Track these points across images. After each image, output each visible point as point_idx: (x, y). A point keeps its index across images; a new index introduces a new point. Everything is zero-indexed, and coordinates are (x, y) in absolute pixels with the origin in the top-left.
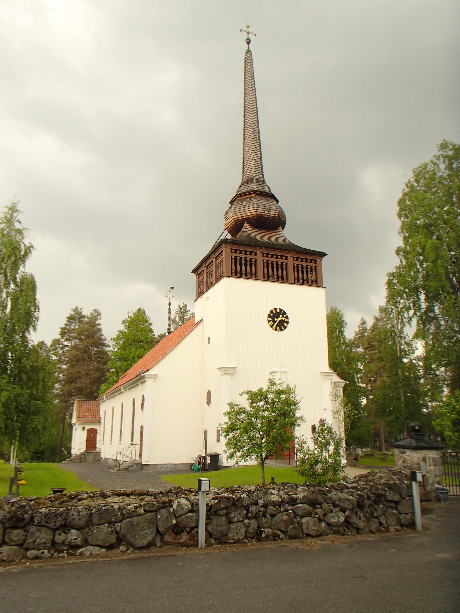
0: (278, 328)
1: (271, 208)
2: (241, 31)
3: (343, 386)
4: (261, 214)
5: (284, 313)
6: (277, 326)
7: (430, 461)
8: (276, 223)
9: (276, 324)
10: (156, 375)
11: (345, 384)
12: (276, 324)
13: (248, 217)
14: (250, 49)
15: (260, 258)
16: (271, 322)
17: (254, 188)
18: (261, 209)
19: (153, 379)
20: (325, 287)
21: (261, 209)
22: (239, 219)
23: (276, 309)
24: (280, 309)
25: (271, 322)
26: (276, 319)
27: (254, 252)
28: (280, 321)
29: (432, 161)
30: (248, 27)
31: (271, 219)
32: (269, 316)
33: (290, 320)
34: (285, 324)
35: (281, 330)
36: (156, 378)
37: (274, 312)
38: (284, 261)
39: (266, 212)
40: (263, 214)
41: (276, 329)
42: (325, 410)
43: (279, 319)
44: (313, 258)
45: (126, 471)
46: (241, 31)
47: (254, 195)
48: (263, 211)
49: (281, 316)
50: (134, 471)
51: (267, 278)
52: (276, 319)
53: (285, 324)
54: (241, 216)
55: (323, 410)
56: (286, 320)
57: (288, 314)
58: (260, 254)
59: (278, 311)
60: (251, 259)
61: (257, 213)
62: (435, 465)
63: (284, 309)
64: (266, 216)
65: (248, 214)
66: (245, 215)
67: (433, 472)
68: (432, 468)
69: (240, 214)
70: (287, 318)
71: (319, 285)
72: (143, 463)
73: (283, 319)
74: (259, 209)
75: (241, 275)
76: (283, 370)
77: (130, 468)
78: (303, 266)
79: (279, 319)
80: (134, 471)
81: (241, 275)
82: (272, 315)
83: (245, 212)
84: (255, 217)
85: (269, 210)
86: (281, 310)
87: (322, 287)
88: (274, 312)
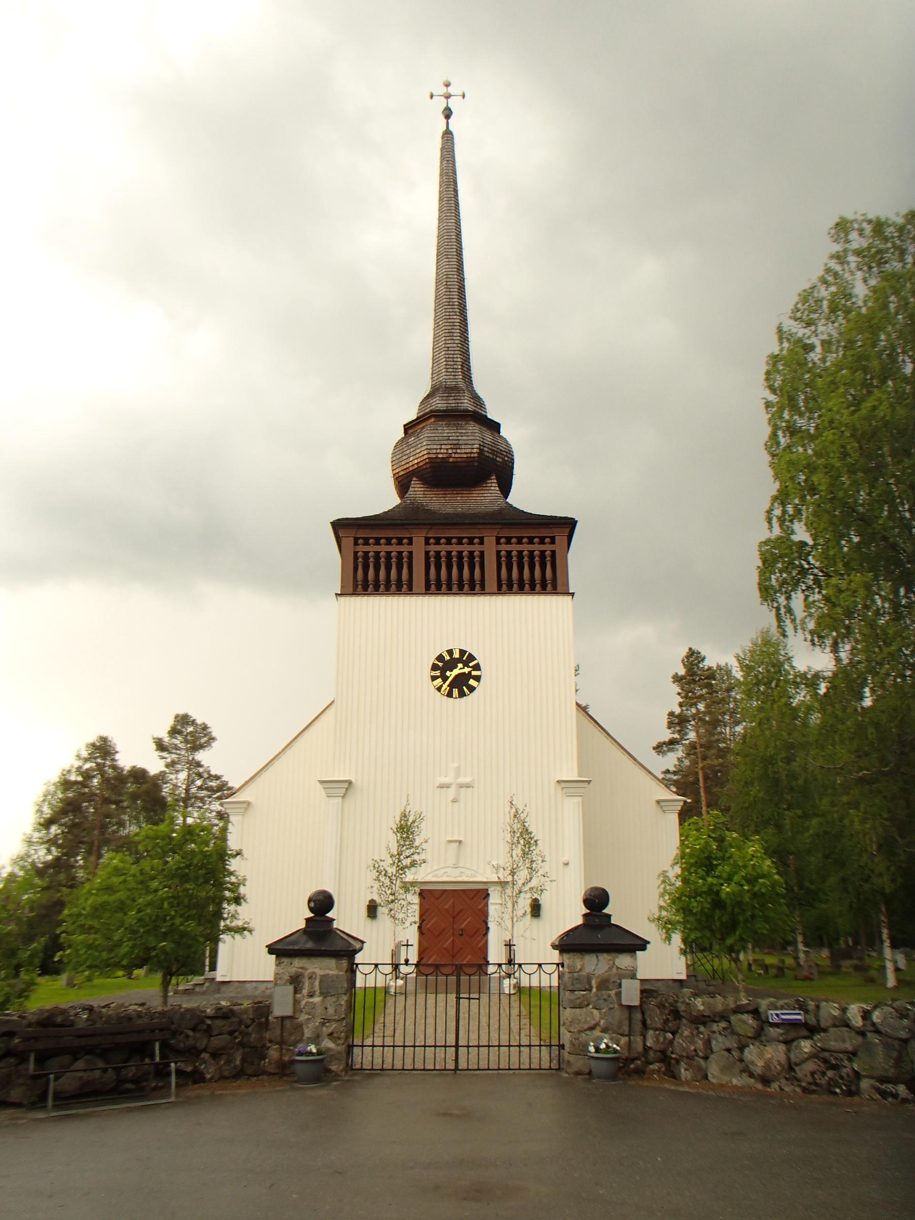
0: (455, 692)
1: (461, 442)
2: (432, 96)
3: (679, 808)
4: (440, 456)
5: (471, 658)
6: (451, 686)
7: (312, 984)
8: (497, 467)
9: (448, 683)
10: (248, 804)
11: (682, 804)
12: (448, 683)
13: (416, 466)
14: (450, 128)
15: (490, 548)
16: (440, 680)
17: (453, 405)
18: (439, 447)
19: (242, 810)
20: (573, 594)
21: (439, 447)
22: (402, 473)
23: (450, 652)
24: (460, 650)
25: (440, 680)
26: (448, 673)
27: (407, 538)
28: (456, 676)
29: (828, 270)
30: (447, 85)
31: (463, 464)
32: (434, 667)
33: (484, 673)
34: (472, 682)
35: (462, 694)
36: (246, 809)
37: (447, 658)
38: (477, 548)
39: (450, 451)
40: (445, 456)
41: (450, 695)
42: (567, 864)
43: (456, 672)
44: (544, 532)
45: (189, 994)
46: (432, 96)
47: (433, 420)
48: (442, 451)
49: (460, 665)
50: (204, 993)
51: (506, 587)
52: (448, 673)
53: (472, 682)
54: (405, 467)
55: (561, 865)
56: (474, 673)
57: (480, 659)
58: (490, 541)
59: (456, 655)
60: (400, 553)
61: (431, 456)
62: (324, 994)
63: (469, 650)
64: (451, 460)
65: (416, 461)
66: (411, 464)
67: (319, 1011)
68: (317, 999)
69: (403, 463)
70: (477, 667)
71: (559, 589)
72: (219, 979)
73: (467, 670)
74: (435, 447)
75: (449, 588)
76: (462, 780)
77: (198, 989)
78: (532, 556)
79: (456, 672)
80: (204, 993)
81: (449, 588)
82: (440, 664)
83: (411, 459)
84: (428, 466)
85: (457, 446)
86: (463, 652)
87: (567, 593)
88: (447, 658)
